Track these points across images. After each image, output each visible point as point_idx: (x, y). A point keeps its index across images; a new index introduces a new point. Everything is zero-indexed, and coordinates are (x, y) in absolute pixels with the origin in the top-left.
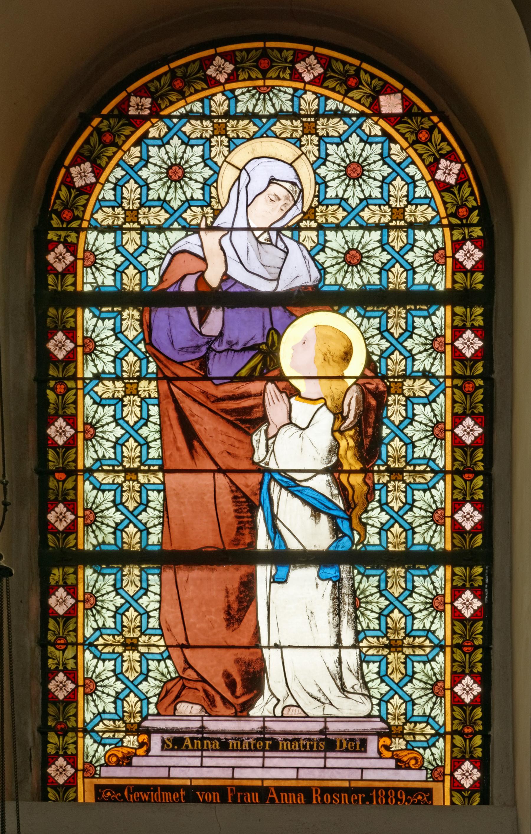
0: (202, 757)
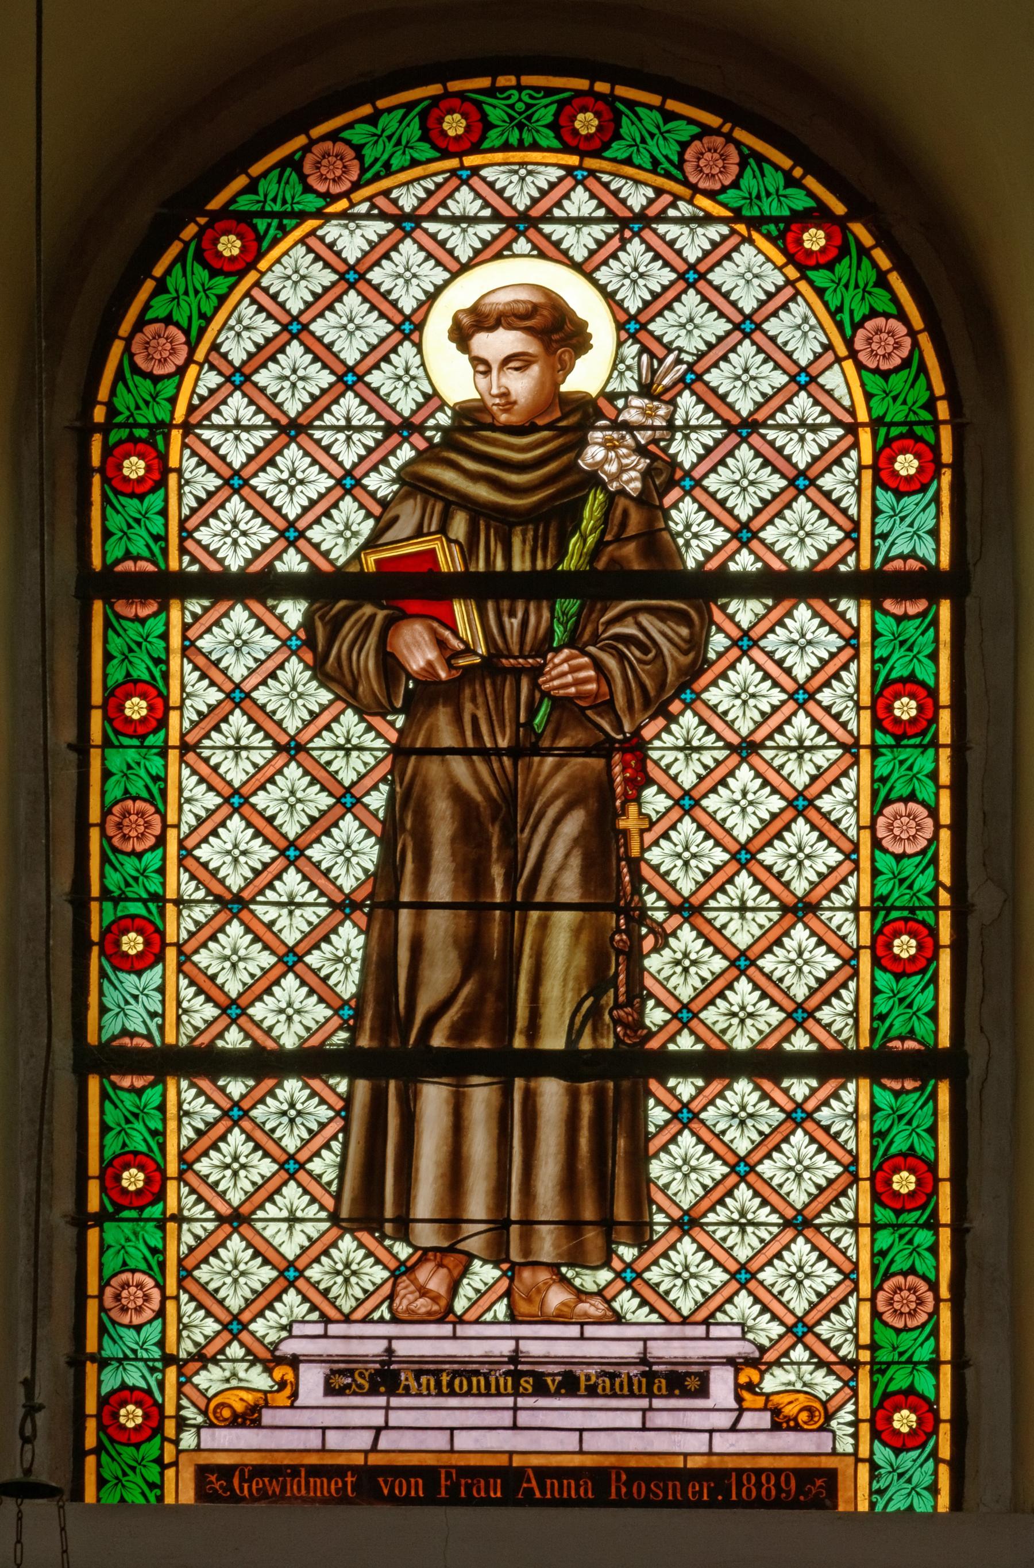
0: (515, 1409)
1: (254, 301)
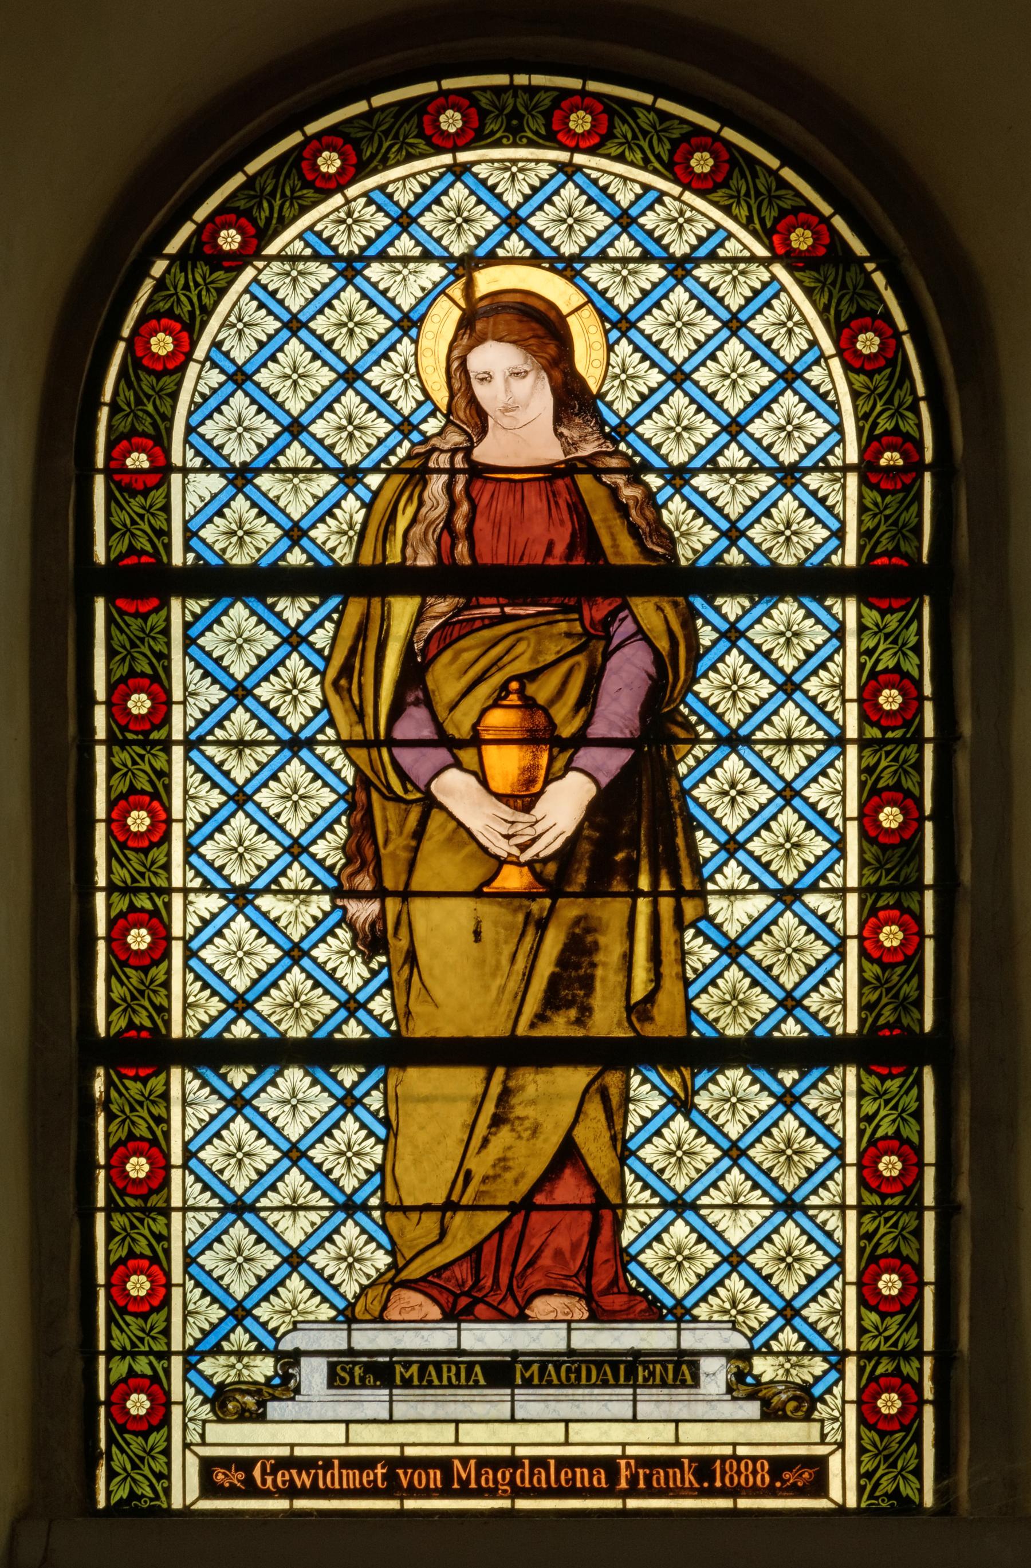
1: (254, 297)
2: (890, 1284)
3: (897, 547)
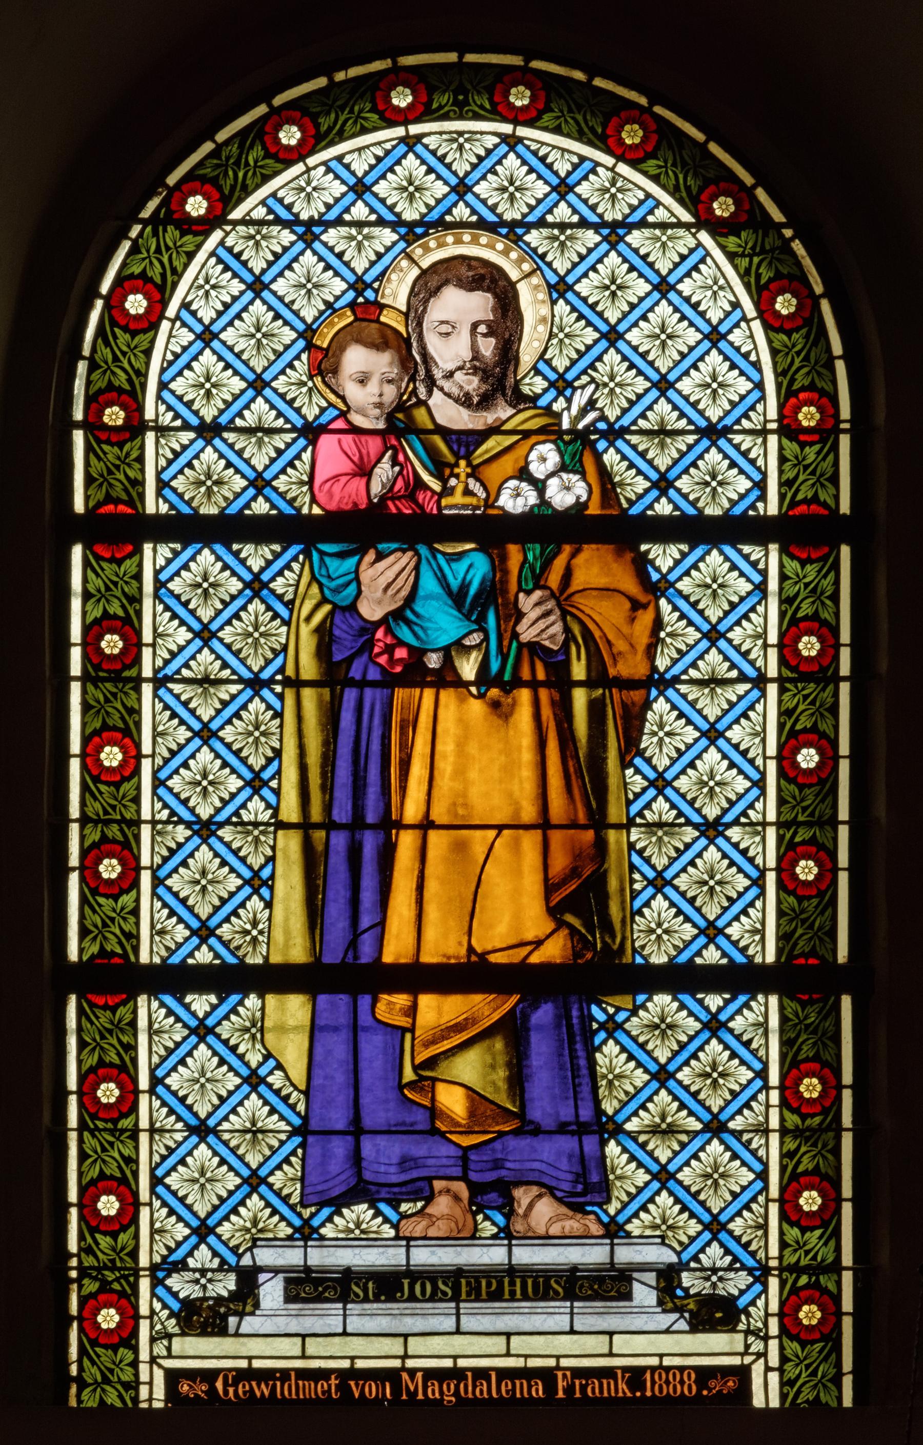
1: (220, 261)
2: (810, 1201)
3: (816, 494)
